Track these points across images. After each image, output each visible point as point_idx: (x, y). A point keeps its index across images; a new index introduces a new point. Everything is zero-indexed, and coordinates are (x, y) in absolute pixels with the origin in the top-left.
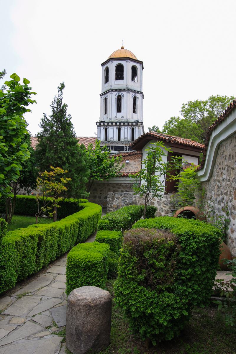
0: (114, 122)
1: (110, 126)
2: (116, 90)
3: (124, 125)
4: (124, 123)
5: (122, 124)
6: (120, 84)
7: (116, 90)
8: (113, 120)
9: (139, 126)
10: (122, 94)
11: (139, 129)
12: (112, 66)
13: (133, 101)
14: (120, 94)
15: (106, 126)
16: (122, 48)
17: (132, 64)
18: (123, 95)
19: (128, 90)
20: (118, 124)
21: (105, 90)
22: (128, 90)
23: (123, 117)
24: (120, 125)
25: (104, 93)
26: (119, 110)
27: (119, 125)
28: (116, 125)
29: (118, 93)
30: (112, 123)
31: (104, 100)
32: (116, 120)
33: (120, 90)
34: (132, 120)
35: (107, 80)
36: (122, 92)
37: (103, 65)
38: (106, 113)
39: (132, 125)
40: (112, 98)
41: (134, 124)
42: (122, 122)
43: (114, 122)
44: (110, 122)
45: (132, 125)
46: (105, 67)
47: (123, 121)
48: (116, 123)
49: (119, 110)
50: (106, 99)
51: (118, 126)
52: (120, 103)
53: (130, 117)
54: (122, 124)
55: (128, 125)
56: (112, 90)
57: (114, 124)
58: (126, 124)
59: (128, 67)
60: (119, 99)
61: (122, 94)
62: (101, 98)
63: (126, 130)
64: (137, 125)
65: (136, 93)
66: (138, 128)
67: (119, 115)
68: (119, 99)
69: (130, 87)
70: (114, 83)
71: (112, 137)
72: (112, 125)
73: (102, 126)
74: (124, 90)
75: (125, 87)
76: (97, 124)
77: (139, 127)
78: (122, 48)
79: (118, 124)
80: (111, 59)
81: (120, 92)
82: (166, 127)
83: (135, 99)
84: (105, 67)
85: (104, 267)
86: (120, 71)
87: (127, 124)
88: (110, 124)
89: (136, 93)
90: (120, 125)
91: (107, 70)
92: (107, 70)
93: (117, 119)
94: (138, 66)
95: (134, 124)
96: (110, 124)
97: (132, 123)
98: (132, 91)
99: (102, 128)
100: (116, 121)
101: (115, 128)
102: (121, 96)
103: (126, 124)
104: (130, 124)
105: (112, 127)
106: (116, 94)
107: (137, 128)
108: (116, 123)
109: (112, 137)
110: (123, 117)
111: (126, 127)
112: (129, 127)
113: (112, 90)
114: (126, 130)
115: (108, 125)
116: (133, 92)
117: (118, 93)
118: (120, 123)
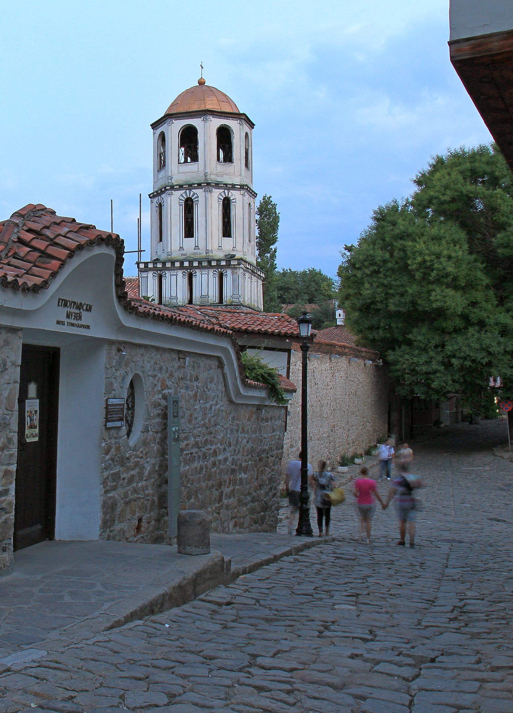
0: (177, 261)
1: (168, 269)
2: (181, 187)
3: (200, 267)
4: (200, 263)
5: (196, 264)
6: (191, 172)
7: (181, 187)
8: (176, 255)
9: (235, 268)
10: (194, 194)
11: (235, 275)
12: (174, 130)
13: (221, 208)
14: (189, 194)
15: (160, 270)
16: (201, 83)
17: (216, 123)
18: (198, 197)
19: (208, 184)
20: (186, 264)
21: (159, 186)
22: (207, 185)
23: (197, 247)
24: (191, 266)
25: (157, 192)
26: (189, 232)
27: (190, 267)
28: (182, 267)
29: (186, 193)
30: (173, 263)
31: (158, 209)
32: (182, 255)
33: (191, 186)
34: (220, 255)
35: (161, 163)
36: (195, 191)
37: (155, 126)
38: (161, 240)
39: (218, 266)
40: (174, 203)
41: (223, 263)
42: (196, 260)
43: (177, 261)
44: (169, 261)
45: (218, 266)
46: (158, 131)
47: (197, 257)
48: (182, 263)
49: (189, 232)
50: (160, 206)
51: (186, 268)
52: (189, 215)
53: (216, 246)
54: (196, 264)
55: (210, 266)
56: (172, 188)
57: (177, 264)
58: (205, 264)
59: (207, 131)
60: (189, 206)
61: (194, 194)
62: (152, 202)
63: (205, 277)
64: (228, 265)
65: (229, 190)
66: (233, 273)
67: (189, 243)
68: (189, 206)
69: (213, 178)
70: (179, 170)
71: (174, 294)
72: (173, 268)
73: (151, 270)
74: (199, 185)
75: (201, 179)
76: (138, 267)
77: (235, 271)
78: (201, 83)
79: (186, 264)
80: (168, 117)
81: (190, 190)
82: (284, 274)
83: (227, 204)
84: (158, 131)
85: (246, 505)
86: (189, 139)
87: (207, 263)
88: (168, 265)
89: (229, 190)
90: (191, 266)
91: (162, 137)
92: (162, 137)
93: (183, 252)
94: (233, 124)
95: (223, 263)
96: (168, 265)
97: (218, 261)
98: (217, 185)
99: (150, 274)
100: (182, 258)
101: (180, 273)
102: (192, 200)
103: (205, 264)
104: (214, 263)
105: (173, 272)
106: (181, 195)
107: (229, 272)
108: (182, 263)
109: (174, 294)
110: (197, 247)
111: (205, 272)
112: (211, 272)
113: (172, 188)
114: (205, 277)
115: (164, 268)
116: (220, 188)
117: (186, 193)
118: (191, 262)
